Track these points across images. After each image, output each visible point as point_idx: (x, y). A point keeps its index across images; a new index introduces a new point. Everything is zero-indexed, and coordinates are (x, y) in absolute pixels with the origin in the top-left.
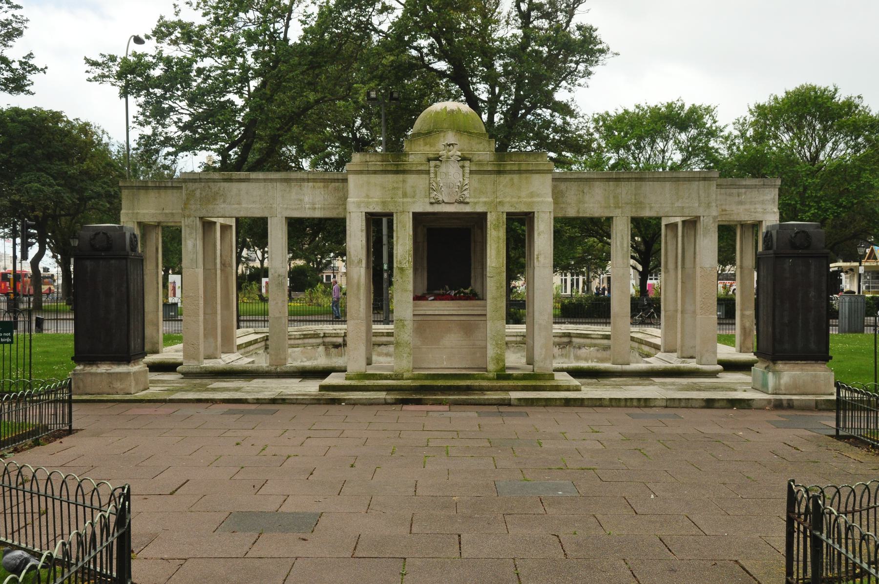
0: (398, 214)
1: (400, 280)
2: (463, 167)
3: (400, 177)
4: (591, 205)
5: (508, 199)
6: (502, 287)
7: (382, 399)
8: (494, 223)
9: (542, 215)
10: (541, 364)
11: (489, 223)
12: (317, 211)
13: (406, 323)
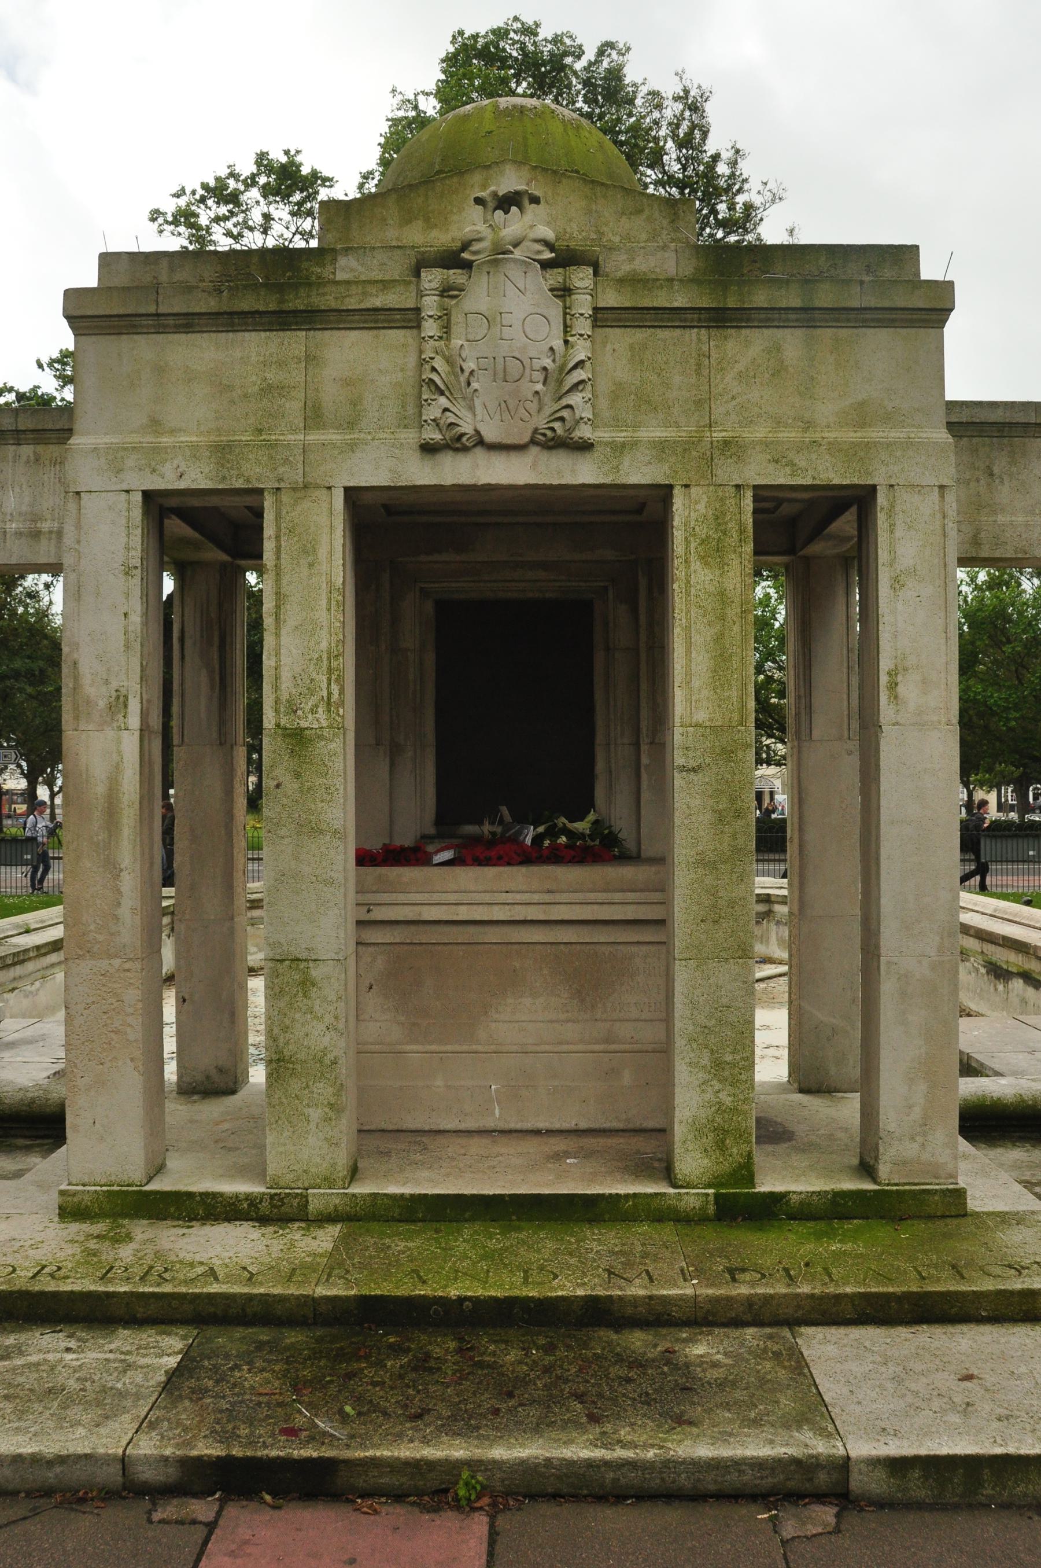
0: (285, 498)
1: (291, 786)
2: (564, 292)
3: (295, 342)
4: (1020, 519)
5: (760, 432)
6: (738, 815)
7: (107, 1460)
8: (702, 531)
9: (907, 500)
10: (910, 1150)
11: (678, 536)
12: (44, 542)
13: (316, 973)
